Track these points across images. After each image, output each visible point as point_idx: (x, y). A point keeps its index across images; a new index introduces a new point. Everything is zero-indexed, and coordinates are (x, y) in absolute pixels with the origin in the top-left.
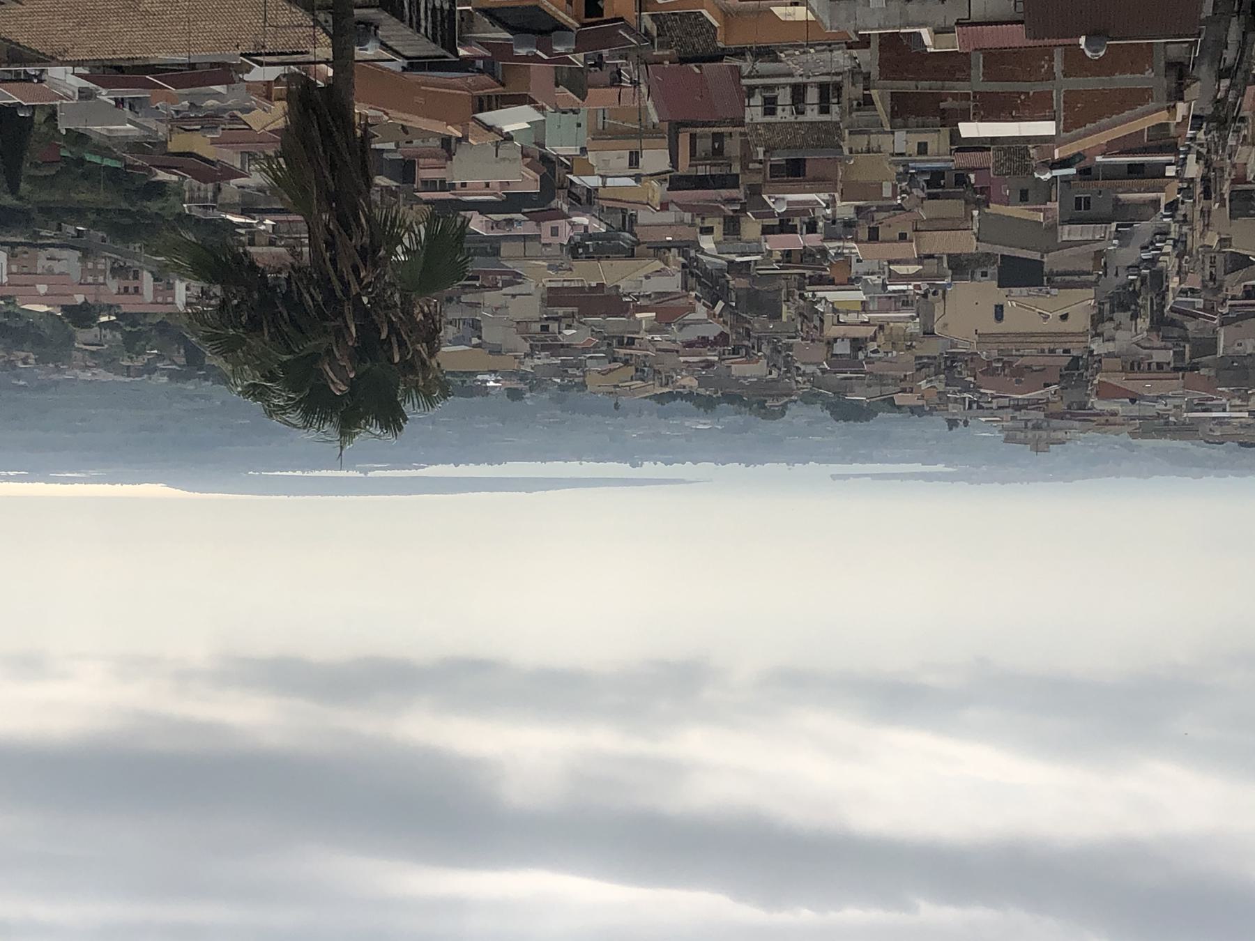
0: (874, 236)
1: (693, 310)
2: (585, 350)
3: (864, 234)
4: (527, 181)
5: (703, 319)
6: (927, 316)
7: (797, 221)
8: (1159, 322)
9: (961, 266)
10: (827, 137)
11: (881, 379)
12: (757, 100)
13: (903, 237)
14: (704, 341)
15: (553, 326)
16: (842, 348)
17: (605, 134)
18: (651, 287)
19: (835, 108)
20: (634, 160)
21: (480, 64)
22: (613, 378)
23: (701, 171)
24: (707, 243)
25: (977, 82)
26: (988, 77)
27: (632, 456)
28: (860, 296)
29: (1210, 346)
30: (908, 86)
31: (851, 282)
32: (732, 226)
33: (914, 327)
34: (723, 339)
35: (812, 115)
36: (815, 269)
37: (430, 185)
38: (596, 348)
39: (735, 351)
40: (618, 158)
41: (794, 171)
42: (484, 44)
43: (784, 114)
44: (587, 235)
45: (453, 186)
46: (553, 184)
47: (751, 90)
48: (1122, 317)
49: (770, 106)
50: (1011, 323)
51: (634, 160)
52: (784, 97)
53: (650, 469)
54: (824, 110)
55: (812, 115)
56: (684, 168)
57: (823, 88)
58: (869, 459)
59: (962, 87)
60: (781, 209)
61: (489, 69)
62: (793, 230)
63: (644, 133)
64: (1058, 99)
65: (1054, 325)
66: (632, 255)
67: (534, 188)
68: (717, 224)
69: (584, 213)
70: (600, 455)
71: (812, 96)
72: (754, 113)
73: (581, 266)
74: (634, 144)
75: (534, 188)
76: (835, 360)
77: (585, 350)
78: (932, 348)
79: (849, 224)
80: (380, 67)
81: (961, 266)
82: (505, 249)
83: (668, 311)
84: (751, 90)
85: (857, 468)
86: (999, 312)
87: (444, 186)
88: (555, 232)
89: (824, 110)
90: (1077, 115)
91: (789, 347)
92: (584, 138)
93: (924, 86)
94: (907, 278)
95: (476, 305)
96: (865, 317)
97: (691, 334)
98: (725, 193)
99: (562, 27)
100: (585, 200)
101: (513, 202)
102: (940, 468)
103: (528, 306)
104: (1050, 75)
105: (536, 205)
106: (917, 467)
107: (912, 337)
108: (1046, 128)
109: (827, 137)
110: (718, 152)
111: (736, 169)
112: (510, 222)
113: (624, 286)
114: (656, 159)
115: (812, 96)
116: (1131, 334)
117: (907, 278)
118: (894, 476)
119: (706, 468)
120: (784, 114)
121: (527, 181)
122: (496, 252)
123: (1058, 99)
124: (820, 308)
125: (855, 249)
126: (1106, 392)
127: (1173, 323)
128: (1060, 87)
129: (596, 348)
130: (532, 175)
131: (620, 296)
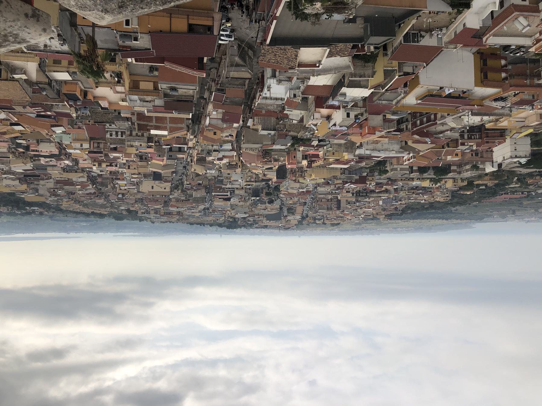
0: (129, 168)
1: (89, 186)
2: (63, 196)
3: (127, 167)
4: (56, 151)
5: (91, 189)
6: (138, 188)
7: (113, 164)
8: (183, 191)
9: (146, 176)
10: (122, 142)
11: (128, 203)
12: (109, 133)
13: (135, 169)
14: (90, 193)
15: (56, 190)
16: (120, 196)
17: (76, 140)
18: (81, 180)
19: (124, 136)
20: (81, 145)
21: (53, 117)
22: (69, 203)
23: (95, 150)
24: (94, 168)
25: (154, 123)
26: (156, 123)
27: (66, 230)
28: (125, 182)
29: (192, 196)
30: (142, 123)
31: (123, 180)
32: (100, 165)
33: (135, 191)
34: (95, 193)
35: (119, 137)
36: (115, 176)
37: (33, 151)
38: (65, 196)
39: (97, 196)
40: (78, 145)
41: (115, 149)
42: (55, 112)
43: (114, 136)
44: (68, 165)
45: (38, 151)
46: (62, 152)
47: (107, 131)
48: (176, 191)
49: (111, 135)
50: (156, 189)
51: (81, 145)
52: (114, 133)
53: (72, 234)
54: (122, 136)
55: (119, 137)
56: (92, 149)
57: (122, 132)
58: (121, 232)
59: (151, 124)
60: (112, 157)
61: (54, 119)
62: (112, 166)
63: (85, 140)
64: (168, 128)
65: (163, 190)
66: (76, 172)
67: (58, 153)
68: (97, 164)
69: (68, 160)
70: (60, 231)
71: (120, 133)
72: (108, 136)
73: (65, 174)
74: (82, 142)
75: (58, 153)
76: (119, 199)
77: (63, 196)
78: (139, 196)
79: (124, 164)
80: (29, 116)
81: (146, 176)
82: (48, 168)
83: (83, 186)
84: (107, 131)
85: (119, 234)
86: (153, 187)
87: (37, 151)
88: (60, 164)
89: (122, 136)
90: (171, 131)
91: (109, 196)
92: (71, 140)
93: (144, 123)
94: (135, 178)
95: (38, 185)
96: (126, 188)
97: (88, 192)
98: (100, 155)
99: (79, 100)
100: (68, 156)
101: (52, 156)
102: (136, 234)
103: (50, 184)
104: (167, 123)
105: (57, 157)
106: (132, 234)
107: (135, 194)
108: (165, 133)
109: (122, 142)
110: (98, 147)
111: (102, 150)
112: (51, 161)
113: (74, 179)
114: (86, 146)
115: (120, 133)
116: (177, 194)
117: (135, 178)
118: (128, 236)
119: (85, 234)
120: (114, 136)
121: (56, 151)
122: (46, 169)
123: (168, 128)
124: (116, 186)
125: (125, 170)
126: (173, 206)
127: (185, 191)
128: (169, 125)
129: (65, 196)
130: (57, 150)
131: (73, 182)
